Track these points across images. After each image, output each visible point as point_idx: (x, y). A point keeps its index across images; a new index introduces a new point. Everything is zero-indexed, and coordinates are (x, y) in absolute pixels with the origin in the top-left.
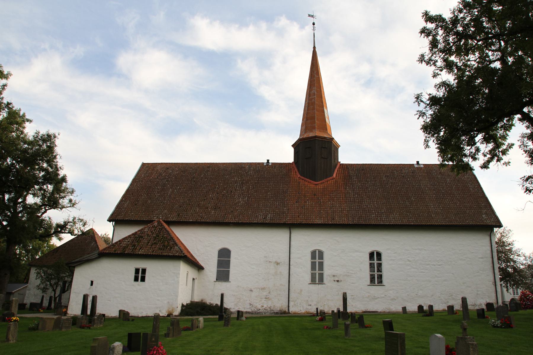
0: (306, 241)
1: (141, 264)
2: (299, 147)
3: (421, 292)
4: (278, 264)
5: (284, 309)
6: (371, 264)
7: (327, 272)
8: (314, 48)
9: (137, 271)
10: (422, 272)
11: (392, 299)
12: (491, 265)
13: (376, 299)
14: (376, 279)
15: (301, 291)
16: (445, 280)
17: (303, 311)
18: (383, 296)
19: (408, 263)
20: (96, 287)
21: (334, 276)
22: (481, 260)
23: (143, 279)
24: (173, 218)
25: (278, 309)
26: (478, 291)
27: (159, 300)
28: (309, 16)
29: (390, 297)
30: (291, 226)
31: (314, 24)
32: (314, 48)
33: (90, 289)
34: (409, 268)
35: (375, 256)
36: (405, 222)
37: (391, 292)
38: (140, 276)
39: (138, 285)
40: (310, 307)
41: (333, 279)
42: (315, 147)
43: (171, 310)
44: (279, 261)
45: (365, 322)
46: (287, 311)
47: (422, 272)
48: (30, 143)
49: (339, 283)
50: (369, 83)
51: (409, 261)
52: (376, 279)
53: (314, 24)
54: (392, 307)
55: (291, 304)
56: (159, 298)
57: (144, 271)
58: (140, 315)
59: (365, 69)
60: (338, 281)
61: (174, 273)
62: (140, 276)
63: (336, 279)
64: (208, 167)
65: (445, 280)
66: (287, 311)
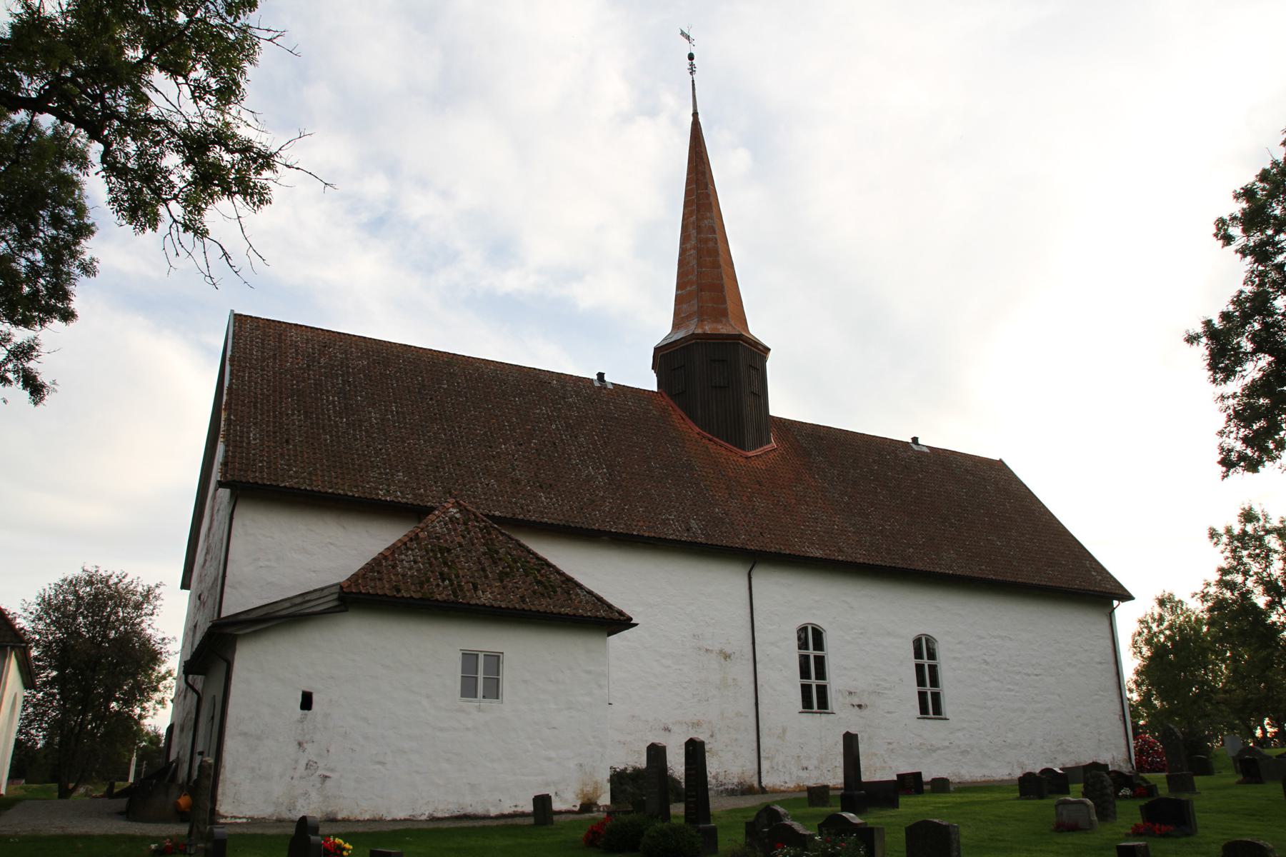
0: (790, 600)
1: (484, 639)
2: (664, 358)
3: (1010, 735)
4: (727, 657)
5: (748, 781)
6: (917, 665)
7: (835, 682)
8: (695, 114)
9: (469, 659)
10: (1009, 690)
11: (964, 752)
12: (1115, 679)
13: (934, 751)
14: (931, 705)
15: (784, 731)
16: (1049, 710)
17: (791, 785)
18: (947, 744)
19: (984, 666)
20: (326, 715)
21: (850, 693)
22: (1099, 667)
23: (493, 690)
24: (546, 506)
25: (736, 781)
26: (1100, 734)
27: (550, 759)
28: (683, 33)
29: (959, 746)
30: (753, 558)
31: (691, 57)
32: (695, 114)
33: (301, 721)
34: (986, 678)
35: (924, 648)
36: (975, 571)
37: (960, 734)
38: (481, 679)
39: (479, 709)
40: (804, 774)
41: (849, 700)
42: (713, 360)
43: (589, 789)
44: (728, 650)
45: (711, 806)
46: (756, 784)
47: (1009, 690)
48: (183, 152)
49: (865, 712)
50: (380, 224)
51: (986, 663)
52: (931, 705)
53: (691, 57)
54: (963, 772)
55: (765, 765)
56: (552, 754)
57: (495, 661)
58: (494, 812)
59: (376, 187)
60: (860, 706)
61: (589, 672)
62: (481, 679)
63: (856, 702)
64: (449, 364)
65: (1049, 710)
66: (756, 784)
